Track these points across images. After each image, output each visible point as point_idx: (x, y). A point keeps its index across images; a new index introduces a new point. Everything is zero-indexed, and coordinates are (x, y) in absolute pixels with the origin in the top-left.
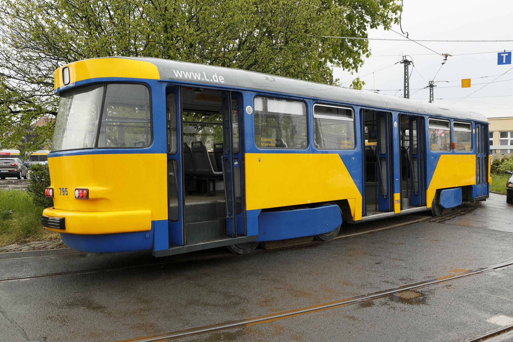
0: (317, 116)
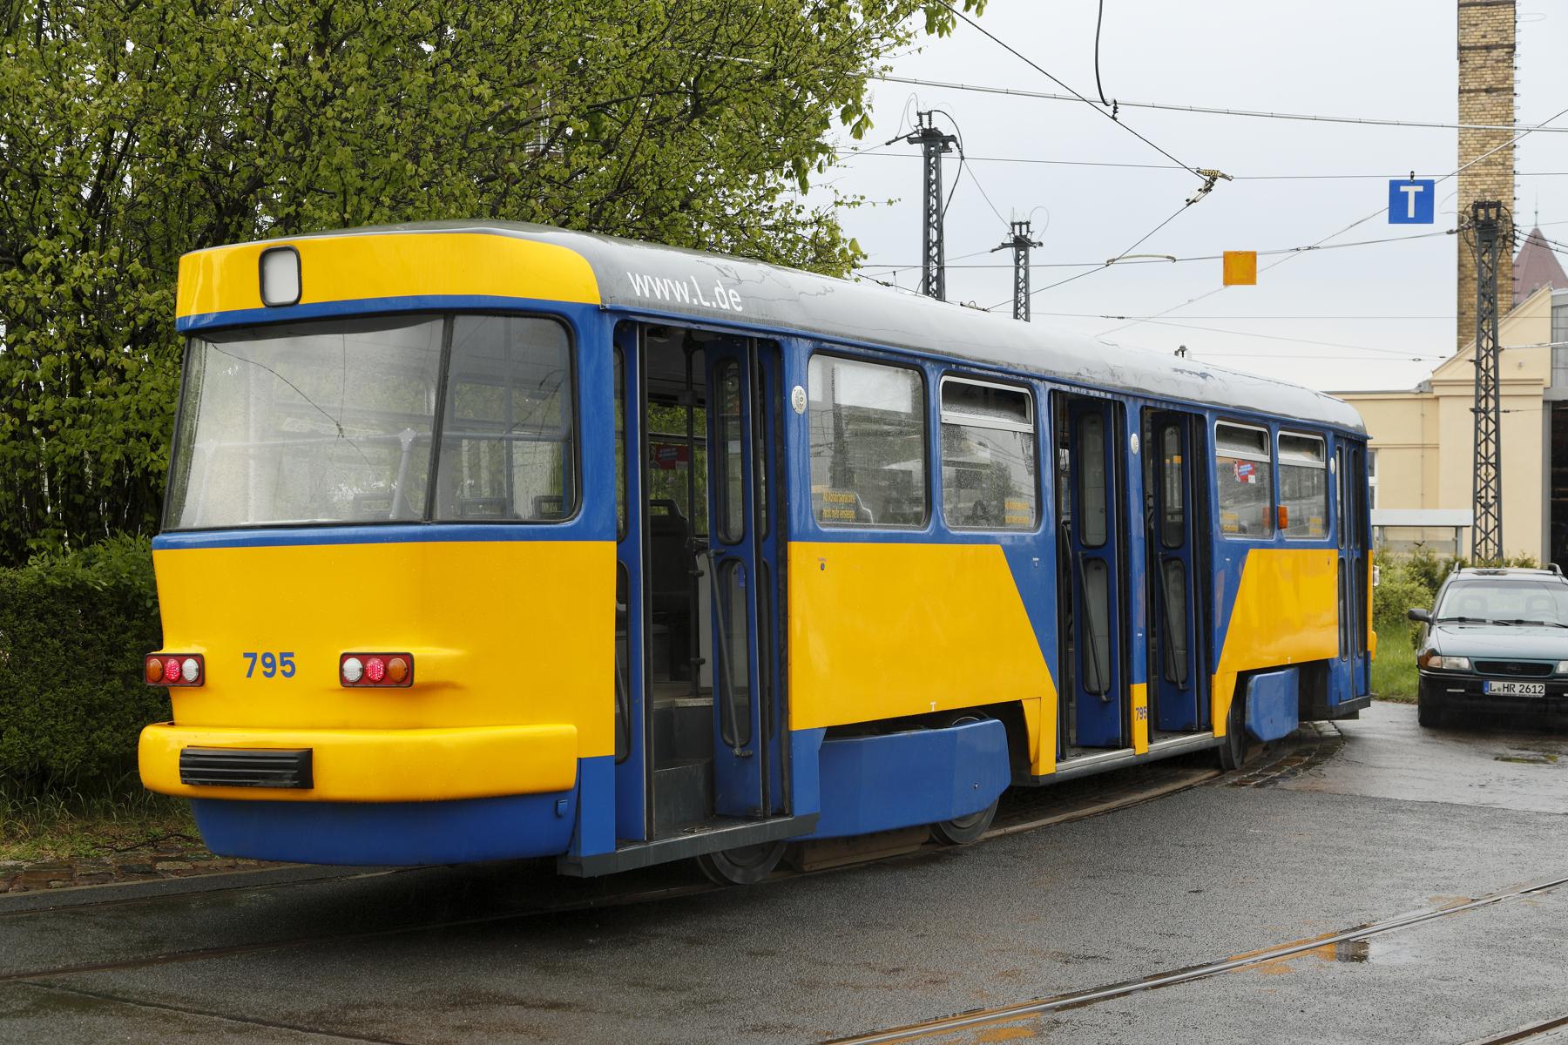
0: (951, 415)
